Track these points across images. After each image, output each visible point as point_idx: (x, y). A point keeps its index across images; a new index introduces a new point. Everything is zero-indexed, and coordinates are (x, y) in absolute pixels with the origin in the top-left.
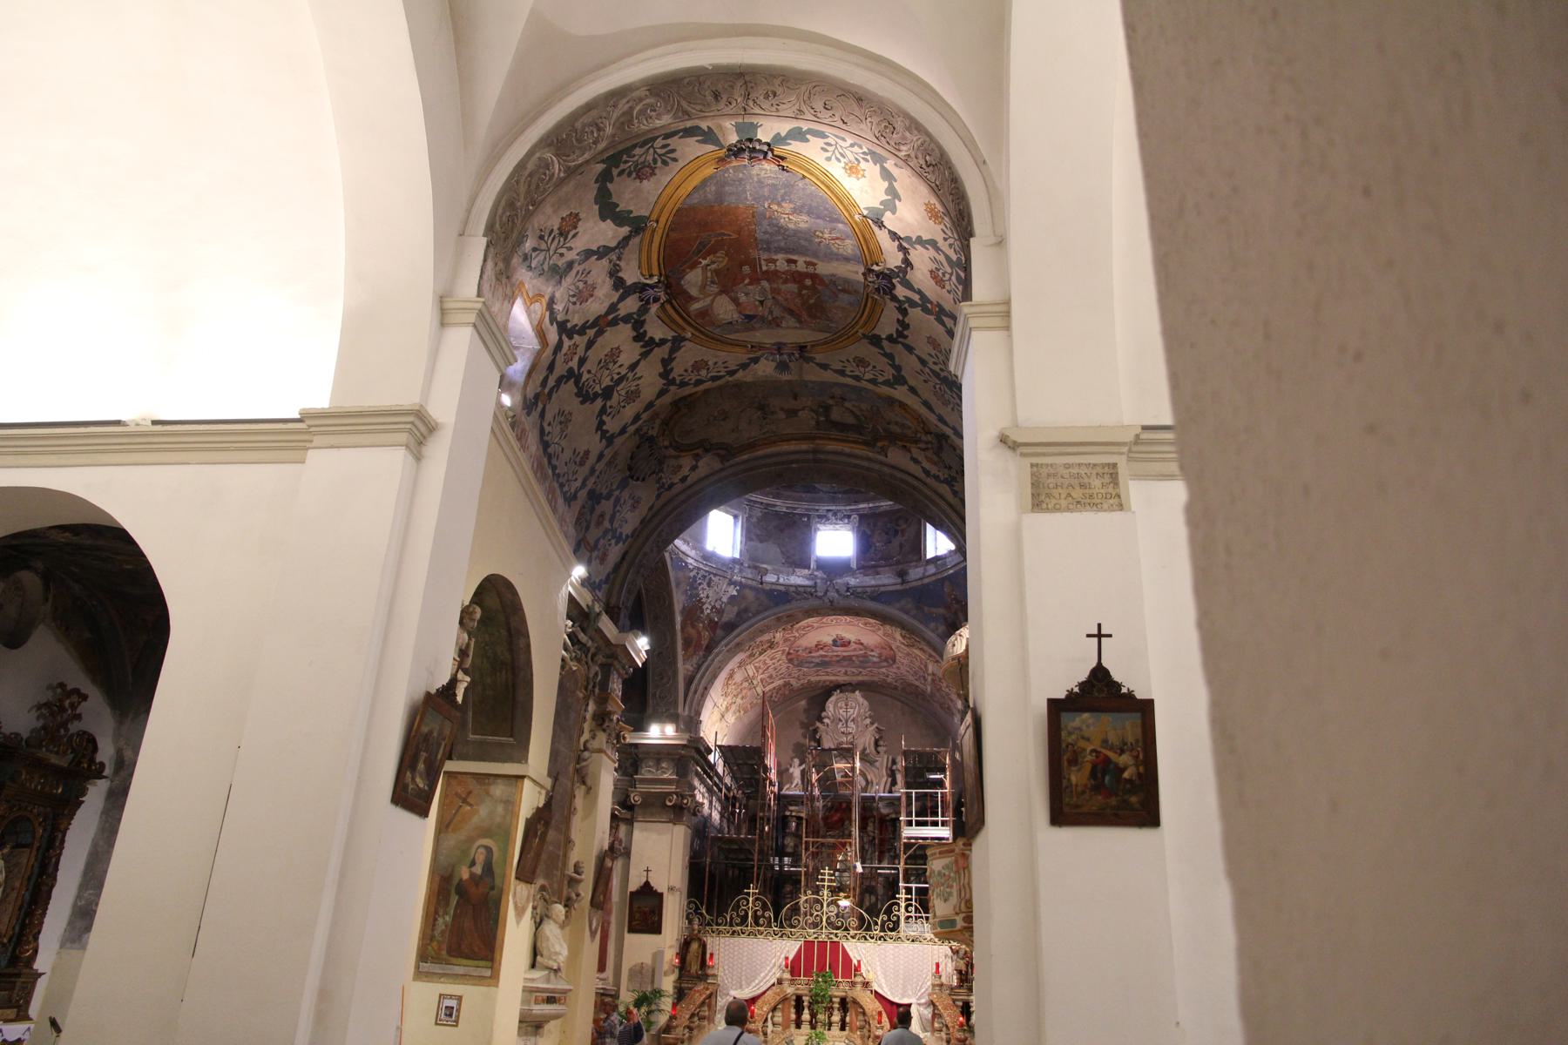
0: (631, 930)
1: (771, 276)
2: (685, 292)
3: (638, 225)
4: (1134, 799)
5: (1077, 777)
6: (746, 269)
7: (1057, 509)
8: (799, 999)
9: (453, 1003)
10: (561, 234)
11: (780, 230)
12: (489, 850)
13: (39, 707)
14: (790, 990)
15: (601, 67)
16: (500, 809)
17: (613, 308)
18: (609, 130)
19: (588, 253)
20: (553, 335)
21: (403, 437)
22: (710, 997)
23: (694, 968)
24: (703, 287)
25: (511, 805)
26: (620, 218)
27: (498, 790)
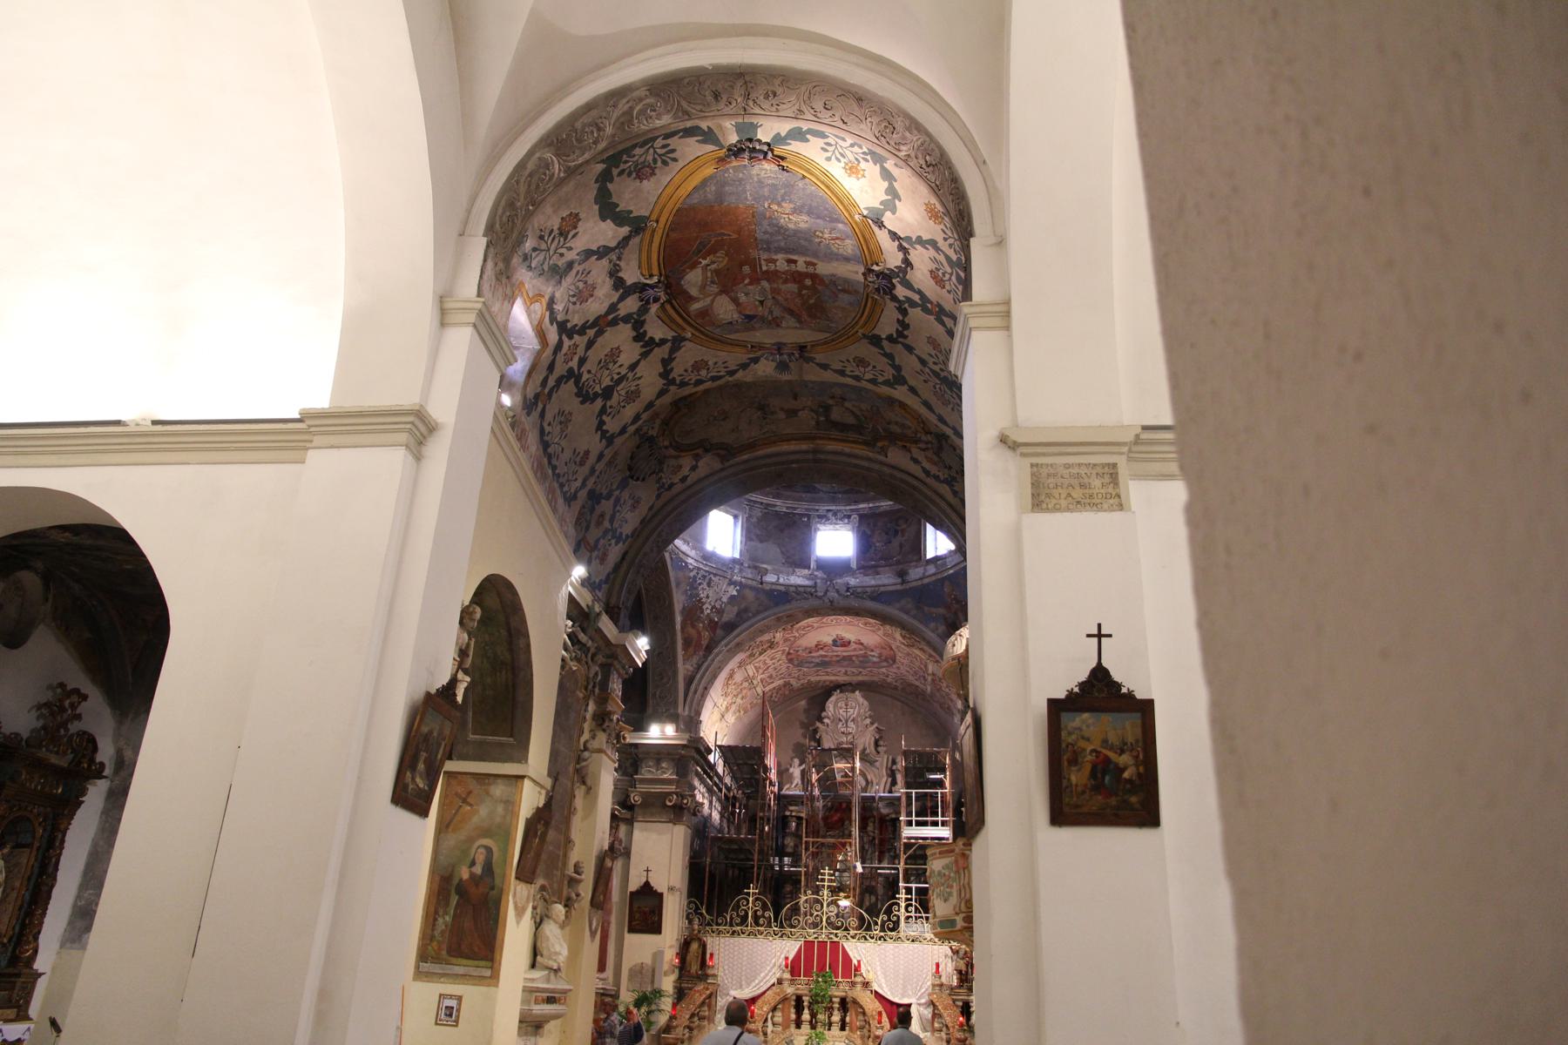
0: (631, 930)
1: (771, 276)
2: (685, 292)
3: (638, 225)
4: (1134, 799)
5: (1077, 777)
6: (746, 269)
7: (1057, 509)
8: (799, 999)
9: (453, 1003)
10: (561, 234)
11: (780, 230)
12: (489, 850)
13: (39, 707)
14: (790, 990)
15: (601, 67)
16: (500, 809)
17: (613, 308)
18: (609, 130)
19: (588, 253)
20: (553, 335)
21: (403, 437)
22: (710, 997)
23: (694, 968)
24: (703, 287)
25: (511, 805)
26: (620, 218)
27: (498, 790)
